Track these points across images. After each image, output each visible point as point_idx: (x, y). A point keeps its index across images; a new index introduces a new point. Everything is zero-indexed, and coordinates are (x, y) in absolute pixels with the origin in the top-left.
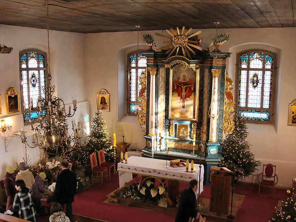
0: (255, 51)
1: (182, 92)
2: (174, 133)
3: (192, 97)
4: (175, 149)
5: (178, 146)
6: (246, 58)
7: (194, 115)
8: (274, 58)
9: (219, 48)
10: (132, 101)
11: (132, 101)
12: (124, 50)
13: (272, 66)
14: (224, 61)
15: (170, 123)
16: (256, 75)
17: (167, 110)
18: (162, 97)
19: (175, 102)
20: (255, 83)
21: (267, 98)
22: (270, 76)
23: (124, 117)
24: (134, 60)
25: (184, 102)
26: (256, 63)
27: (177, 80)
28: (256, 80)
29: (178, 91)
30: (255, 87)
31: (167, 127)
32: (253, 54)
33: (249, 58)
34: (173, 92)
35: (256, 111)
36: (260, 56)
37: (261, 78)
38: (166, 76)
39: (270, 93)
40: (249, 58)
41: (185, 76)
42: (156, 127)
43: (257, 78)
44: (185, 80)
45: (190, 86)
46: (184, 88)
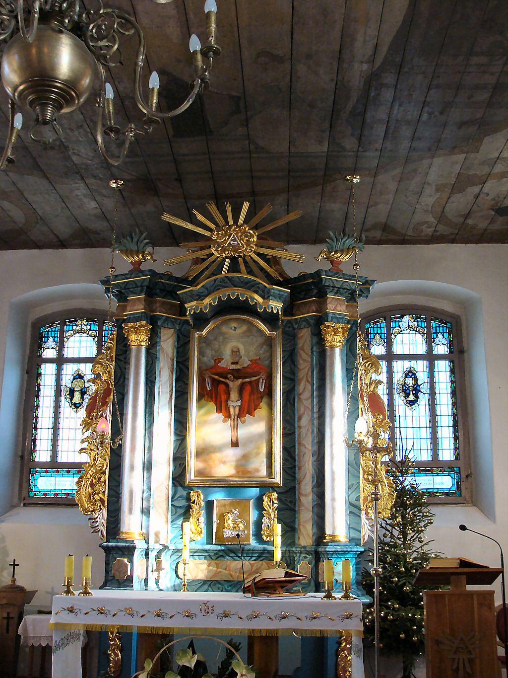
0: (403, 310)
1: (228, 398)
2: (204, 531)
3: (262, 411)
4: (209, 584)
5: (216, 574)
6: (380, 327)
7: (270, 466)
8: (453, 326)
9: (340, 267)
10: (37, 460)
11: (37, 460)
12: (24, 308)
13: (450, 348)
14: (351, 306)
15: (188, 499)
16: (410, 371)
17: (179, 460)
18: (164, 415)
19: (209, 427)
20: (411, 393)
21: (446, 432)
22: (448, 374)
23: (7, 512)
24: (51, 339)
25: (235, 427)
26: (409, 341)
27: (213, 362)
28: (413, 387)
29: (216, 398)
30: (411, 403)
31: (182, 511)
32: (398, 318)
33: (388, 328)
34: (200, 397)
35: (420, 471)
36: (418, 322)
37: (427, 380)
38: (178, 352)
39: (454, 418)
40: (388, 328)
41: (238, 351)
42: (146, 511)
43: (416, 379)
44: (237, 363)
45: (254, 379)
46: (234, 385)
